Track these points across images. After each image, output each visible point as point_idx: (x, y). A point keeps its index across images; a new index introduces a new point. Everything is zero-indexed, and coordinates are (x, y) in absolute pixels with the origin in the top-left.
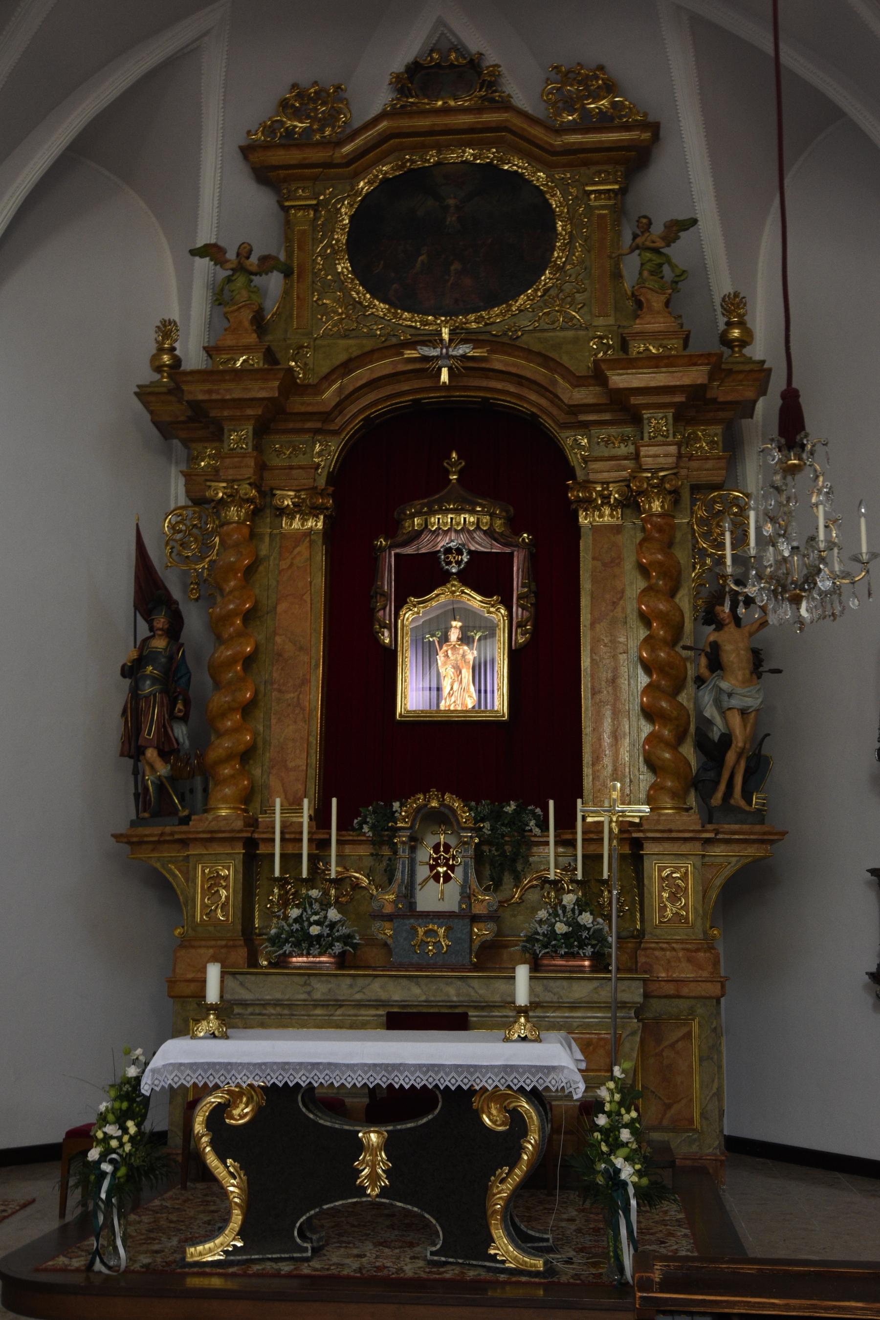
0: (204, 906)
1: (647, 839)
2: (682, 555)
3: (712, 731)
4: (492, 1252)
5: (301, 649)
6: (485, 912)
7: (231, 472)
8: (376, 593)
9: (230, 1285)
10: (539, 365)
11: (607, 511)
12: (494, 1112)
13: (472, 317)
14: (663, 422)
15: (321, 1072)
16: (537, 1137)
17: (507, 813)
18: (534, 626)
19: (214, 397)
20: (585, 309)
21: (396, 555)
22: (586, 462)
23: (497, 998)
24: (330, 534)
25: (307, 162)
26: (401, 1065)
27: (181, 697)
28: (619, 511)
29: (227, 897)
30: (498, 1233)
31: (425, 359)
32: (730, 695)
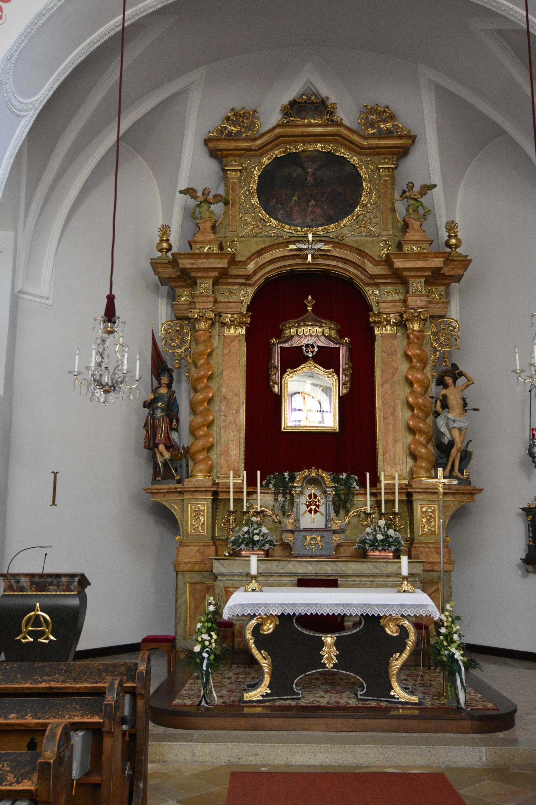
0: (192, 525)
1: (415, 492)
2: (428, 350)
3: (444, 439)
4: (392, 694)
5: (236, 395)
6: (339, 529)
7: (201, 304)
8: (271, 366)
9: (265, 711)
10: (356, 254)
11: (389, 328)
12: (391, 626)
13: (320, 228)
14: (419, 285)
15: (311, 608)
16: (414, 639)
17: (342, 479)
18: (351, 384)
19: (195, 266)
20: (377, 226)
21: (280, 347)
22: (378, 303)
23: (351, 572)
24: (249, 337)
25: (238, 148)
26: (350, 604)
27: (175, 418)
28: (395, 328)
29: (204, 521)
30: (395, 685)
31: (300, 250)
32: (454, 421)
